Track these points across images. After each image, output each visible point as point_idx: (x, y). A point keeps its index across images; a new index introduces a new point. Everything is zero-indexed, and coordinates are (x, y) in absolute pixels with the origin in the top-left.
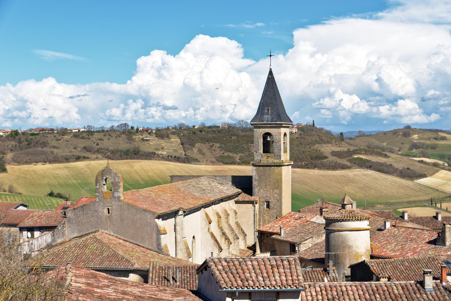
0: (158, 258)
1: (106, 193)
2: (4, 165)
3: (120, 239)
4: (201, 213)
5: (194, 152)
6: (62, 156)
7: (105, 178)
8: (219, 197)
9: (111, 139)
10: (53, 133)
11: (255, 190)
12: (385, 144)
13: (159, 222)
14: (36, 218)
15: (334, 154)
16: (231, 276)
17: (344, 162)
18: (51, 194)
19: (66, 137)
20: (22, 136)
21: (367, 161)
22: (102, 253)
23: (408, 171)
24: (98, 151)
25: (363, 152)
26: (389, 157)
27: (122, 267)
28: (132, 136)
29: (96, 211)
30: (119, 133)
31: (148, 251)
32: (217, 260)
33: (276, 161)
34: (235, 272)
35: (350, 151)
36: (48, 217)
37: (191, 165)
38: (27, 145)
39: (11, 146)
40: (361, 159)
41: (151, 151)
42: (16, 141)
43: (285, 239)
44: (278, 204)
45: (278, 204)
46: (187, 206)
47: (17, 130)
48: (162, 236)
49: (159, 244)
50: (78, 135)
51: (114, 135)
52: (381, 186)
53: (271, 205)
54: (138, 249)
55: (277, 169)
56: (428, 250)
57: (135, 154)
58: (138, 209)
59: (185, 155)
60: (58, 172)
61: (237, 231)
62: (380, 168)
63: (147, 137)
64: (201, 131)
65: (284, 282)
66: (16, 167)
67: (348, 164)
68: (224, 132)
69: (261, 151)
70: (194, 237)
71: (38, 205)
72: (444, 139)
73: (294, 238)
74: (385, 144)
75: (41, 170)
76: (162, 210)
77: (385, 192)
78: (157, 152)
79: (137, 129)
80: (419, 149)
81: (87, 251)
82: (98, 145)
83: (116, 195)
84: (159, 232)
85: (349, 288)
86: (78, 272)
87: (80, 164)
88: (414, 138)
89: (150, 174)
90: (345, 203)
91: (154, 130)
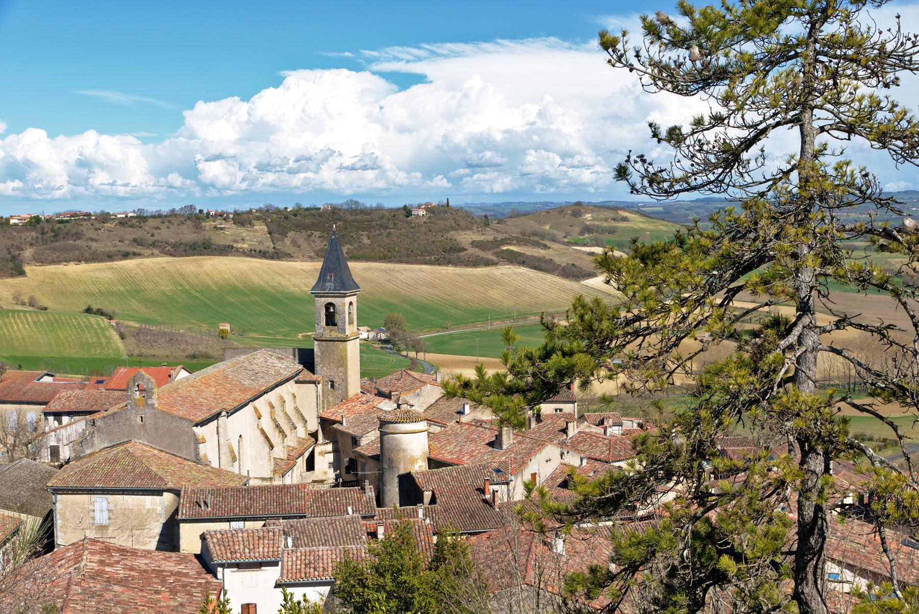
0: (196, 471)
1: (139, 400)
2: (21, 267)
3: (155, 449)
4: (249, 408)
5: (286, 245)
6: (104, 252)
7: (137, 384)
8: (272, 384)
9: (172, 228)
10: (90, 219)
11: (318, 368)
12: (547, 227)
13: (198, 430)
14: (63, 400)
15: (475, 244)
16: (223, 548)
17: (489, 255)
18: (88, 310)
19: (109, 225)
20: (46, 225)
21: (520, 254)
22: (134, 469)
23: (573, 268)
24: (154, 245)
25: (514, 242)
26: (549, 248)
27: (155, 487)
28: (200, 224)
29: (128, 419)
30: (183, 219)
31: (185, 462)
32: (213, 533)
33: (341, 335)
34: (226, 544)
35: (496, 241)
36: (78, 399)
37: (282, 262)
38: (54, 236)
39: (30, 238)
40: (512, 252)
41: (227, 244)
42: (37, 232)
43: (346, 431)
44: (344, 384)
45: (344, 384)
46: (230, 404)
47: (38, 216)
48: (201, 446)
49: (197, 454)
50: (124, 222)
51: (175, 222)
52: (536, 289)
53: (336, 385)
54: (174, 460)
55: (341, 345)
56: (484, 454)
57: (205, 248)
58: (174, 417)
59: (274, 248)
60: (98, 274)
61: (295, 419)
62: (537, 264)
63: (221, 224)
64: (295, 215)
65: (266, 554)
66: (38, 268)
67: (494, 258)
68: (326, 215)
69: (323, 323)
70: (240, 436)
71: (70, 326)
72: (625, 219)
73: (355, 429)
74: (547, 227)
75: (74, 272)
76: (200, 417)
77: (542, 297)
78: (235, 246)
79: (208, 213)
80: (592, 233)
81: (118, 467)
82: (153, 235)
83: (150, 402)
84: (197, 441)
85: (325, 552)
86: (93, 547)
87: (129, 264)
88: (586, 219)
89: (226, 276)
90: (400, 403)
91: (231, 214)
